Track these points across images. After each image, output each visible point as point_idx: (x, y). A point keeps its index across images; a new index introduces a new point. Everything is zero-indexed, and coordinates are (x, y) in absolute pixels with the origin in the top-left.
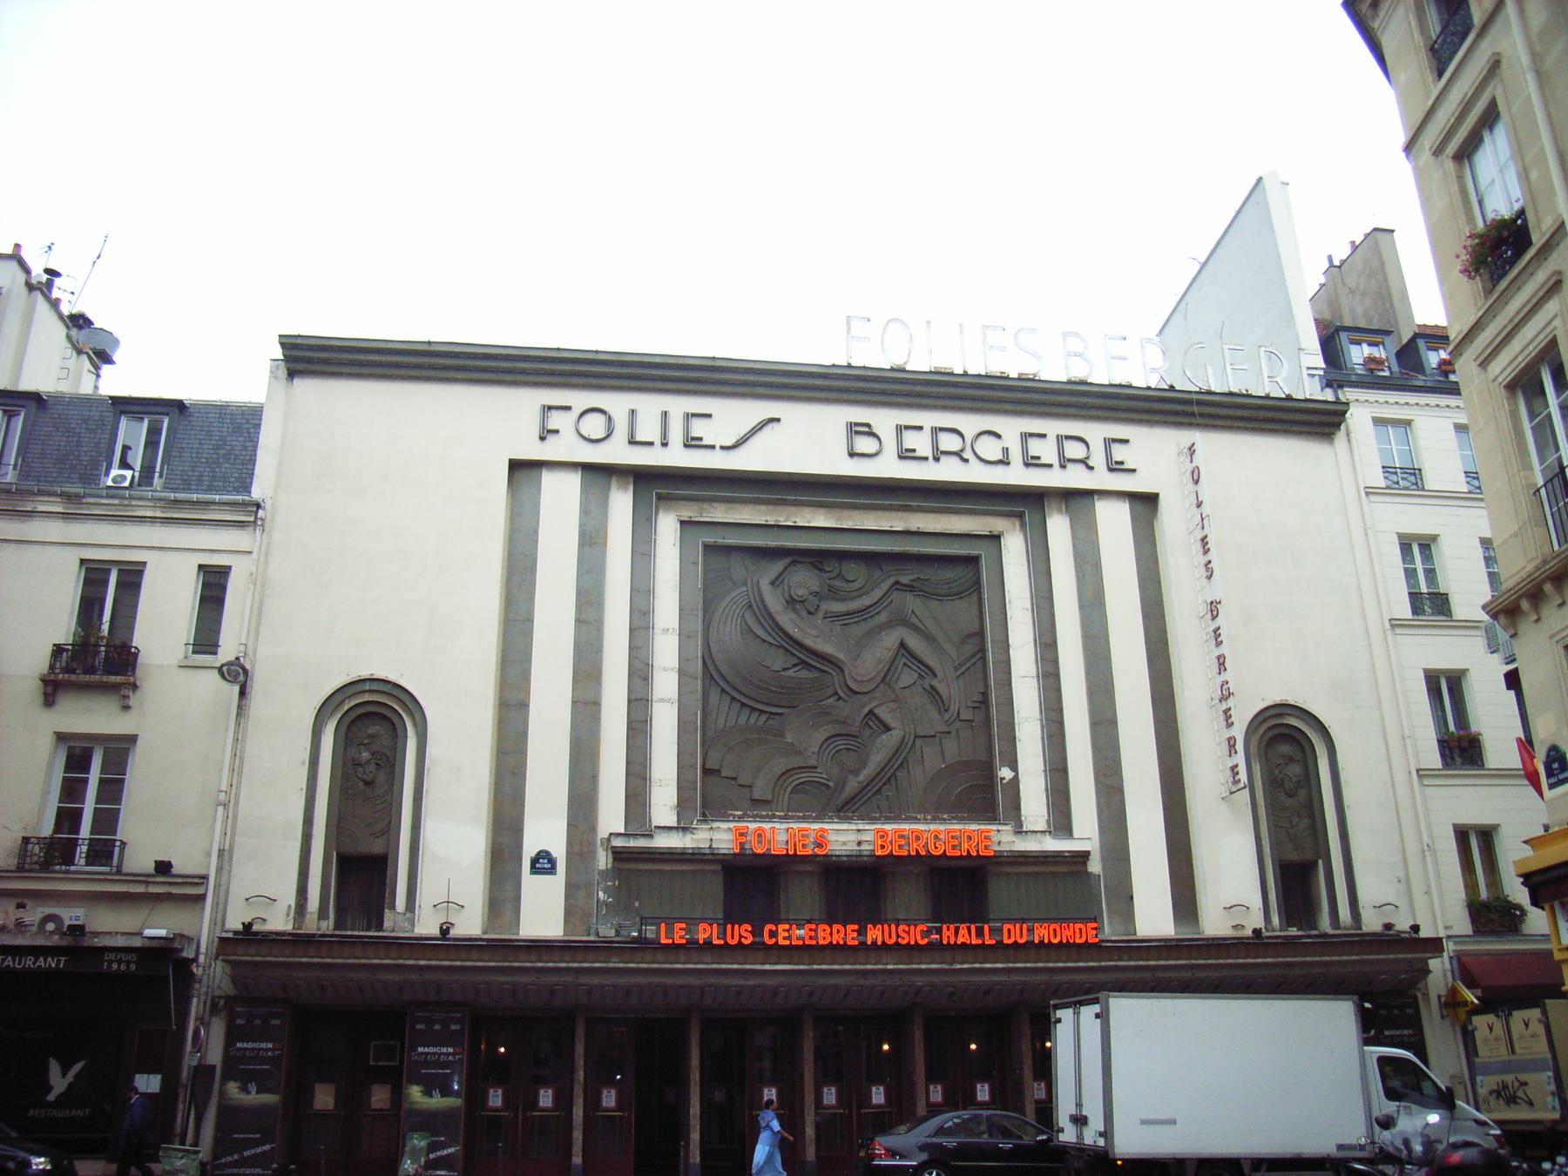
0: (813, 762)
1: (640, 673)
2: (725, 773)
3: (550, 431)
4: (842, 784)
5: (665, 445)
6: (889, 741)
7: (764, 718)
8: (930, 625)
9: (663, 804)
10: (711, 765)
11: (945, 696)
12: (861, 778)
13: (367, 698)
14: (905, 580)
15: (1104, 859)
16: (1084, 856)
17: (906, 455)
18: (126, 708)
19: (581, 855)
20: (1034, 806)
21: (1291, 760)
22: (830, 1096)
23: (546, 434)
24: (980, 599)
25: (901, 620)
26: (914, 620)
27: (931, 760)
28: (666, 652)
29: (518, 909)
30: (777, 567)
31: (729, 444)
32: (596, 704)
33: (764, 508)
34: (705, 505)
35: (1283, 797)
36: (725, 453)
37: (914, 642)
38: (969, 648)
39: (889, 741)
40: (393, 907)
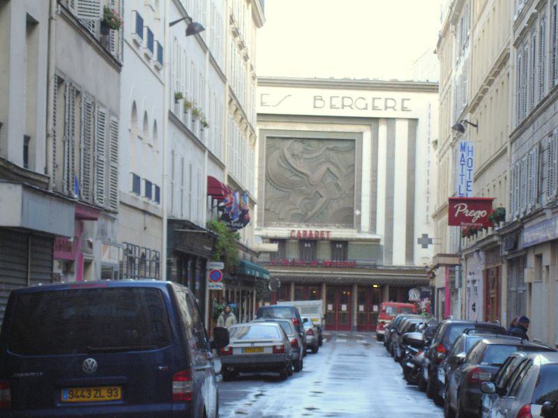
2: (271, 210)
4: (306, 214)
6: (322, 201)
7: (283, 193)
10: (267, 207)
15: (386, 241)
16: (378, 240)
22: (362, 308)
25: (328, 161)
26: (333, 161)
27: (335, 206)
37: (333, 169)
38: (350, 170)
39: (322, 201)
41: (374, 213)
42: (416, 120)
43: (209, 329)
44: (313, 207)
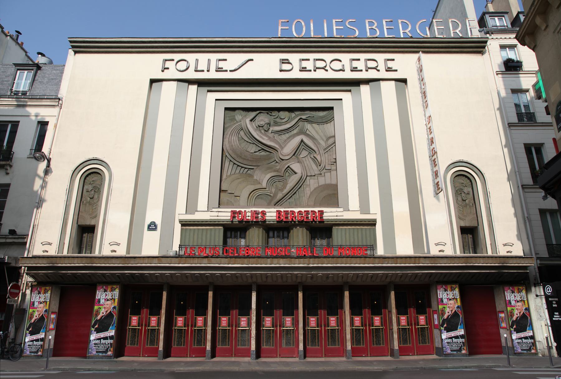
3: (369, 68)
4: (275, 195)
5: (208, 71)
11: (319, 160)
12: (283, 193)
14: (304, 117)
18: (7, 174)
20: (354, 202)
23: (164, 69)
25: (302, 132)
27: (312, 184)
30: (253, 114)
42: (404, 81)
43: (58, 369)
44: (284, 187)
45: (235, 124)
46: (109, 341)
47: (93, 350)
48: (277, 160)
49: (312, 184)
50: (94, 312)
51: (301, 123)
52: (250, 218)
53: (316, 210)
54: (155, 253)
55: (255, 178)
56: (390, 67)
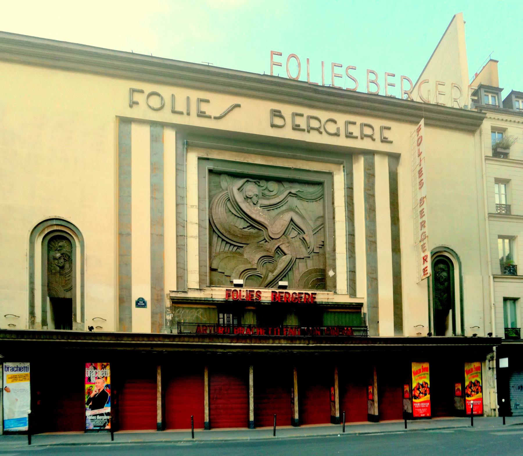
0: (255, 267)
1: (181, 224)
2: (219, 270)
4: (266, 277)
8: (303, 213)
9: (193, 280)
10: (214, 266)
11: (308, 242)
12: (274, 274)
13: (55, 228)
14: (293, 191)
16: (360, 305)
17: (296, 128)
19: (157, 300)
20: (342, 284)
21: (443, 270)
23: (133, 104)
24: (324, 201)
25: (290, 209)
26: (297, 210)
27: (301, 268)
28: (193, 215)
29: (131, 322)
30: (240, 182)
31: (218, 115)
32: (162, 236)
33: (234, 153)
34: (209, 150)
35: (439, 285)
36: (216, 121)
37: (297, 220)
38: (319, 223)
40: (76, 321)
41: (352, 272)
45: (220, 192)
46: (105, 417)
47: (90, 425)
48: (266, 239)
49: (301, 268)
50: (86, 391)
51: (290, 199)
52: (244, 298)
53: (310, 292)
54: (147, 330)
55: (245, 256)
56: (387, 137)
